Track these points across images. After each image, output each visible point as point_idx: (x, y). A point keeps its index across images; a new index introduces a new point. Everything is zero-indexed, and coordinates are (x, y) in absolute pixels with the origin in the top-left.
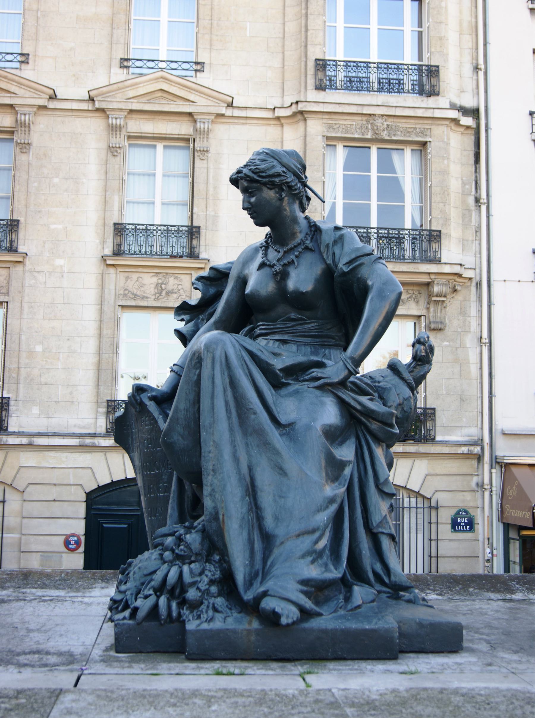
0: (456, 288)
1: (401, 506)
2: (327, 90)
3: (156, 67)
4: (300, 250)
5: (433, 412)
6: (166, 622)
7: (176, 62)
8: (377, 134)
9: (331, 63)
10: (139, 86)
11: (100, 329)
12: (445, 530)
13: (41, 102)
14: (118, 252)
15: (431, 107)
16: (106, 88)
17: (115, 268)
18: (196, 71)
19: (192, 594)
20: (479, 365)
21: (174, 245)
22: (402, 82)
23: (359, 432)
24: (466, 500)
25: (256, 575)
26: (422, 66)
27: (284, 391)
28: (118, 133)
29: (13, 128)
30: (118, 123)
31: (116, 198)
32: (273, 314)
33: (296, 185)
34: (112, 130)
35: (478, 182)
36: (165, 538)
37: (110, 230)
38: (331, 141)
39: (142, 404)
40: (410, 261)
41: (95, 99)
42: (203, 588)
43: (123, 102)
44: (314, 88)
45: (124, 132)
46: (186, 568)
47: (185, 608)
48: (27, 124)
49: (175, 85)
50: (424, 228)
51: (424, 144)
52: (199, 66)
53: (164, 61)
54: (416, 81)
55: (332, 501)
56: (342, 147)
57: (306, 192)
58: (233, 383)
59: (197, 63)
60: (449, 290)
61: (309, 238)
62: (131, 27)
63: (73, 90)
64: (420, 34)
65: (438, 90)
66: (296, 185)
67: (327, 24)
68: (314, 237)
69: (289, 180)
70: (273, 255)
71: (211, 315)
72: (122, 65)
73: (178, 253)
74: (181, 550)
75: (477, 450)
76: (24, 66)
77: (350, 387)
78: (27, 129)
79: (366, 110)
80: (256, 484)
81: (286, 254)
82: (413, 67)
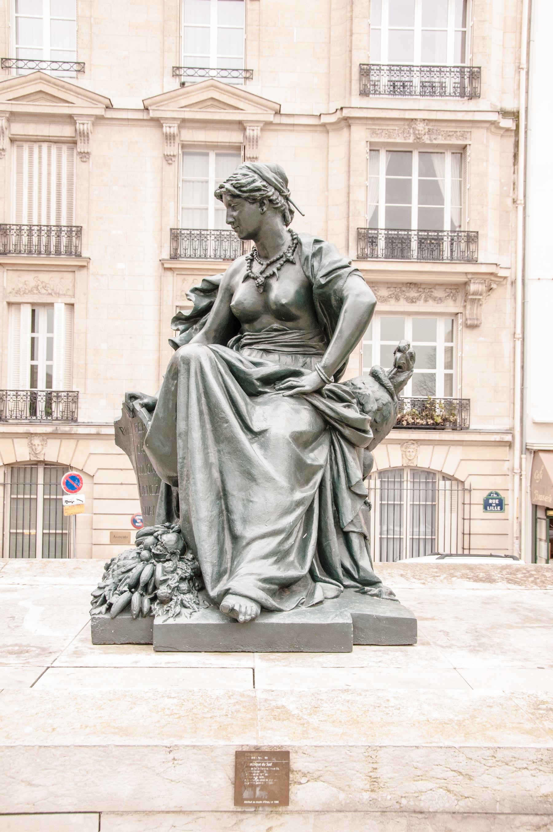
0: (492, 286)
1: (437, 488)
2: (371, 96)
3: (207, 75)
4: (282, 262)
5: (468, 402)
6: (138, 616)
7: (237, 70)
8: (419, 138)
9: (375, 67)
10: (191, 94)
11: (159, 327)
12: (478, 511)
13: (100, 112)
14: (175, 257)
15: (472, 110)
16: (160, 97)
17: (172, 271)
18: (246, 78)
19: (163, 591)
20: (512, 359)
21: (227, 248)
22: (444, 85)
23: (334, 438)
24: (496, 484)
25: (225, 572)
26: (464, 67)
27: (260, 399)
28: (172, 141)
29: (73, 137)
30: (172, 132)
31: (172, 205)
32: (257, 325)
33: (277, 199)
34: (167, 139)
35: (516, 183)
36: (145, 537)
37: (167, 236)
38: (374, 149)
39: (133, 412)
40: (449, 261)
41: (149, 108)
42: (173, 586)
43: (176, 111)
44: (359, 93)
45: (177, 140)
46: (159, 567)
47: (156, 604)
48: (86, 134)
49: (225, 93)
50: (462, 230)
51: (465, 147)
52: (248, 75)
53: (214, 69)
54: (458, 83)
55: (299, 504)
56: (385, 152)
57: (289, 205)
58: (207, 393)
59: (246, 71)
60: (484, 288)
61: (291, 251)
62: (182, 34)
63: (128, 100)
64: (464, 33)
65: (479, 92)
66: (277, 199)
67: (372, 27)
68: (296, 250)
69: (270, 194)
70: (257, 268)
71: (204, 324)
72: (174, 74)
73: (230, 257)
74: (158, 549)
75: (508, 438)
76: (80, 75)
77: (326, 394)
78: (86, 139)
79: (409, 115)
80: (227, 489)
81: (269, 267)
82: (456, 69)
